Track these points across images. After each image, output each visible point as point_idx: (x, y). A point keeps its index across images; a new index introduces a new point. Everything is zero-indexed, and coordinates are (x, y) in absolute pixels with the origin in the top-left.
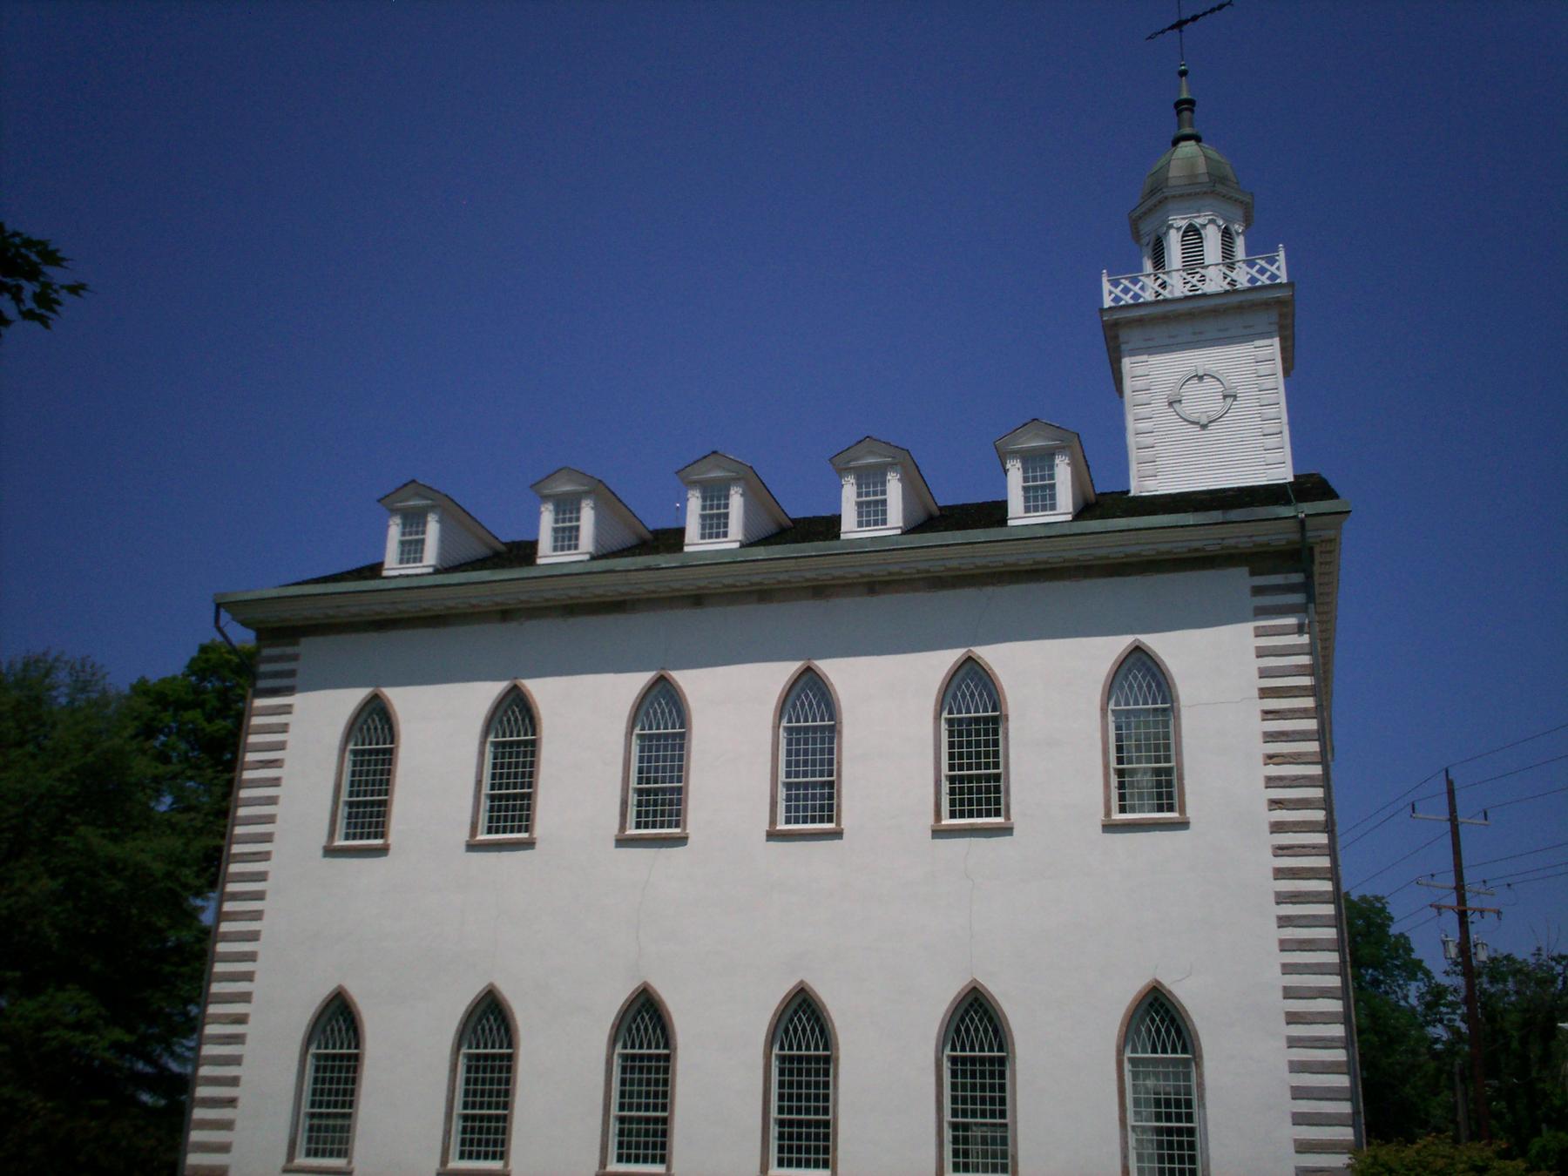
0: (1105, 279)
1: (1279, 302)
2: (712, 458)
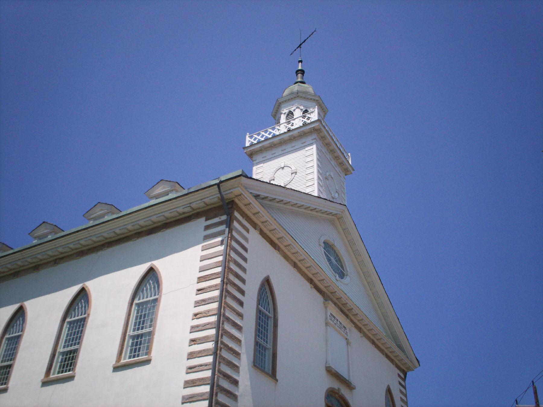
0: (247, 137)
1: (316, 130)
2: (43, 225)
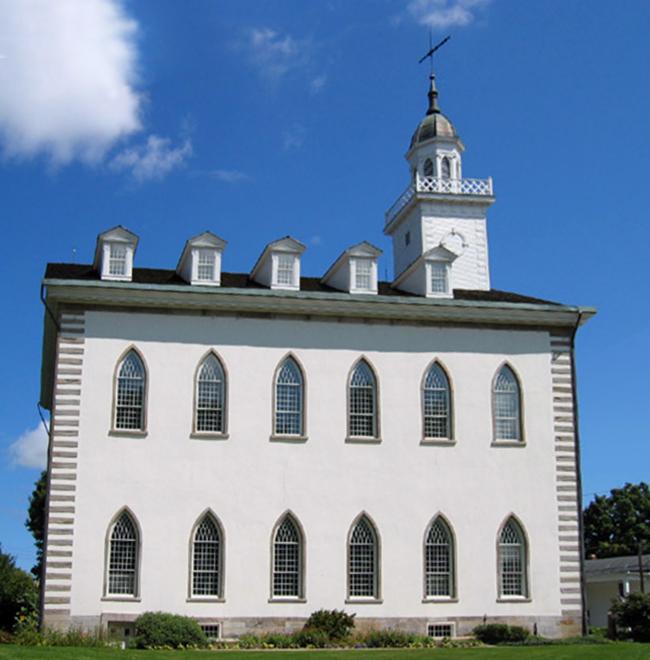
2: (287, 240)
